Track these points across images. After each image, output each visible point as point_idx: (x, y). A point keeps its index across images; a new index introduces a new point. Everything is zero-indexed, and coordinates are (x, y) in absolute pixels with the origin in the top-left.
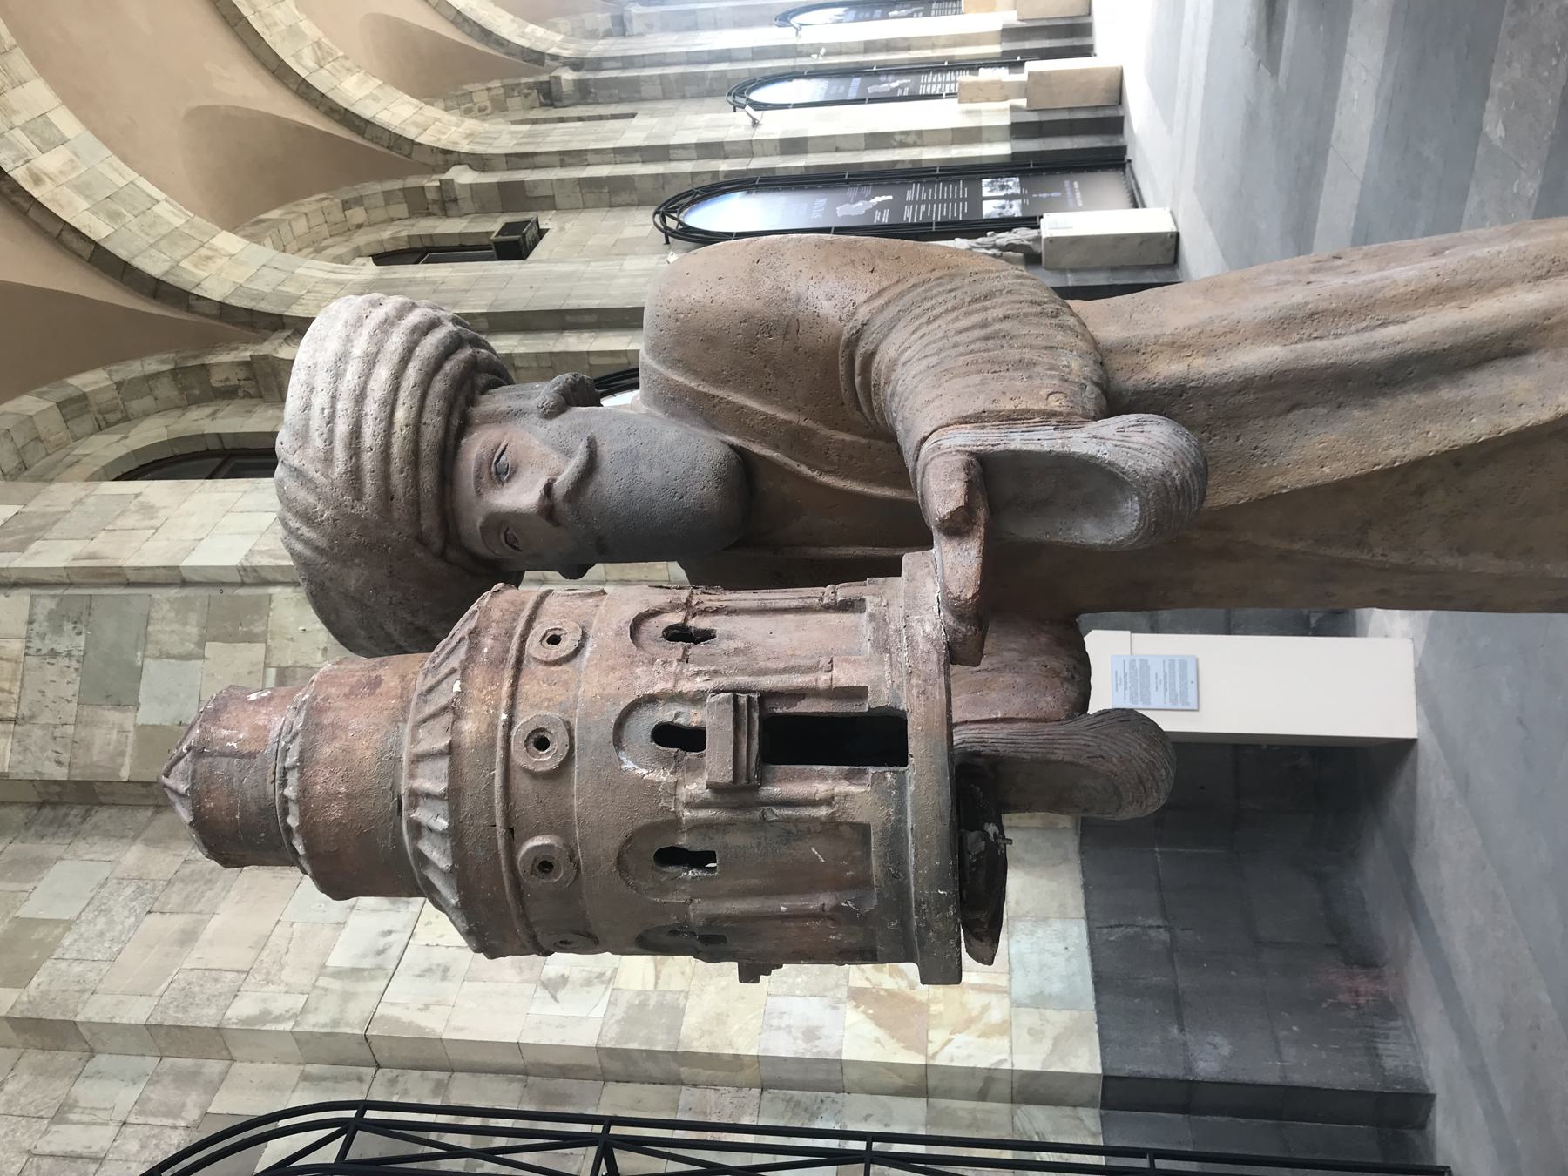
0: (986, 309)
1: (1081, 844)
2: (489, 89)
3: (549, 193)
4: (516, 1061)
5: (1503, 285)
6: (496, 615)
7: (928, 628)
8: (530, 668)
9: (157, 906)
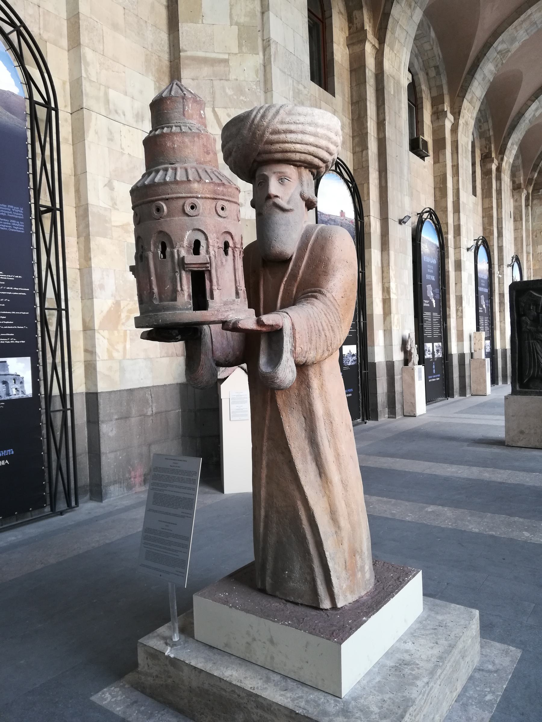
0: (329, 330)
1: (180, 384)
2: (489, 130)
3: (440, 161)
5: (340, 472)
6: (230, 190)
7: (231, 316)
8: (214, 202)
9: (127, 11)
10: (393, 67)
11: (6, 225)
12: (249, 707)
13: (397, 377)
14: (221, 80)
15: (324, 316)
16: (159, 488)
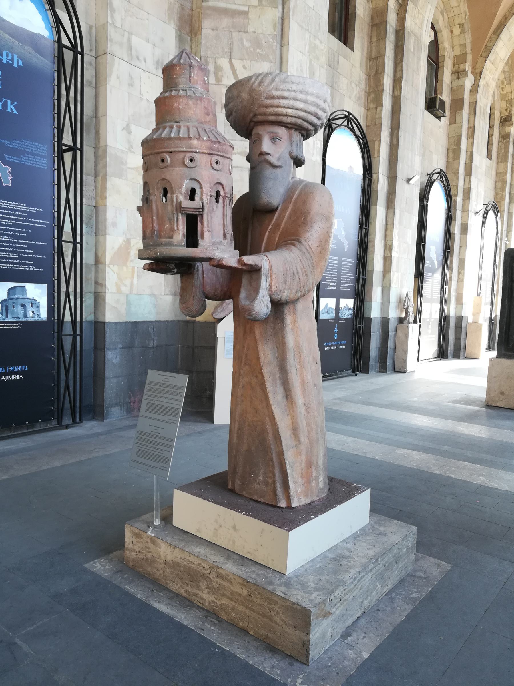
4: (100, 114)
6: (224, 147)
7: (217, 254)
8: (210, 157)
10: (416, 24)
11: (31, 160)
12: (211, 576)
13: (391, 334)
14: (239, 31)
15: (299, 261)
16: (152, 398)
